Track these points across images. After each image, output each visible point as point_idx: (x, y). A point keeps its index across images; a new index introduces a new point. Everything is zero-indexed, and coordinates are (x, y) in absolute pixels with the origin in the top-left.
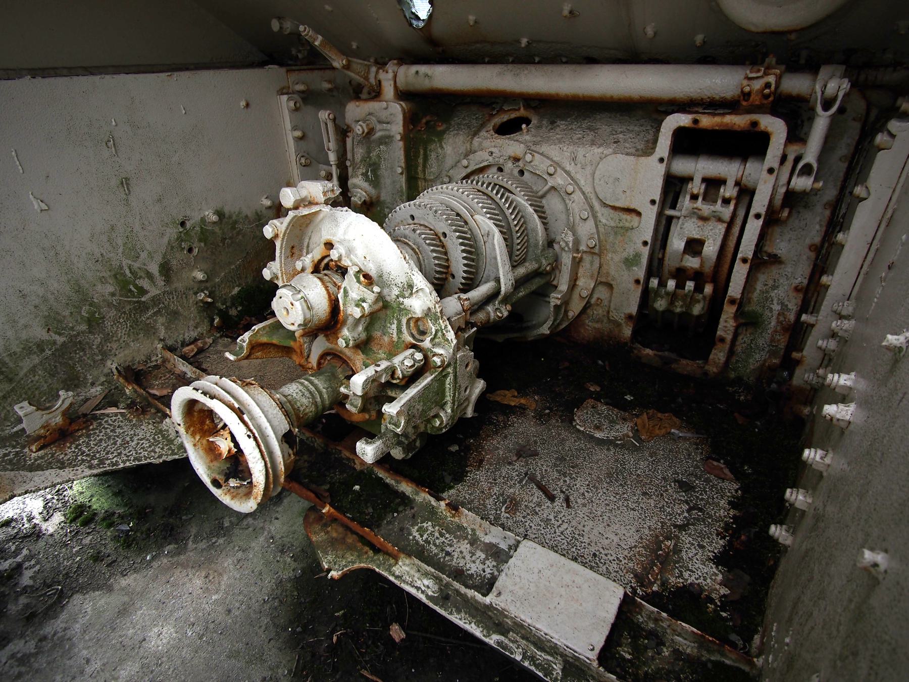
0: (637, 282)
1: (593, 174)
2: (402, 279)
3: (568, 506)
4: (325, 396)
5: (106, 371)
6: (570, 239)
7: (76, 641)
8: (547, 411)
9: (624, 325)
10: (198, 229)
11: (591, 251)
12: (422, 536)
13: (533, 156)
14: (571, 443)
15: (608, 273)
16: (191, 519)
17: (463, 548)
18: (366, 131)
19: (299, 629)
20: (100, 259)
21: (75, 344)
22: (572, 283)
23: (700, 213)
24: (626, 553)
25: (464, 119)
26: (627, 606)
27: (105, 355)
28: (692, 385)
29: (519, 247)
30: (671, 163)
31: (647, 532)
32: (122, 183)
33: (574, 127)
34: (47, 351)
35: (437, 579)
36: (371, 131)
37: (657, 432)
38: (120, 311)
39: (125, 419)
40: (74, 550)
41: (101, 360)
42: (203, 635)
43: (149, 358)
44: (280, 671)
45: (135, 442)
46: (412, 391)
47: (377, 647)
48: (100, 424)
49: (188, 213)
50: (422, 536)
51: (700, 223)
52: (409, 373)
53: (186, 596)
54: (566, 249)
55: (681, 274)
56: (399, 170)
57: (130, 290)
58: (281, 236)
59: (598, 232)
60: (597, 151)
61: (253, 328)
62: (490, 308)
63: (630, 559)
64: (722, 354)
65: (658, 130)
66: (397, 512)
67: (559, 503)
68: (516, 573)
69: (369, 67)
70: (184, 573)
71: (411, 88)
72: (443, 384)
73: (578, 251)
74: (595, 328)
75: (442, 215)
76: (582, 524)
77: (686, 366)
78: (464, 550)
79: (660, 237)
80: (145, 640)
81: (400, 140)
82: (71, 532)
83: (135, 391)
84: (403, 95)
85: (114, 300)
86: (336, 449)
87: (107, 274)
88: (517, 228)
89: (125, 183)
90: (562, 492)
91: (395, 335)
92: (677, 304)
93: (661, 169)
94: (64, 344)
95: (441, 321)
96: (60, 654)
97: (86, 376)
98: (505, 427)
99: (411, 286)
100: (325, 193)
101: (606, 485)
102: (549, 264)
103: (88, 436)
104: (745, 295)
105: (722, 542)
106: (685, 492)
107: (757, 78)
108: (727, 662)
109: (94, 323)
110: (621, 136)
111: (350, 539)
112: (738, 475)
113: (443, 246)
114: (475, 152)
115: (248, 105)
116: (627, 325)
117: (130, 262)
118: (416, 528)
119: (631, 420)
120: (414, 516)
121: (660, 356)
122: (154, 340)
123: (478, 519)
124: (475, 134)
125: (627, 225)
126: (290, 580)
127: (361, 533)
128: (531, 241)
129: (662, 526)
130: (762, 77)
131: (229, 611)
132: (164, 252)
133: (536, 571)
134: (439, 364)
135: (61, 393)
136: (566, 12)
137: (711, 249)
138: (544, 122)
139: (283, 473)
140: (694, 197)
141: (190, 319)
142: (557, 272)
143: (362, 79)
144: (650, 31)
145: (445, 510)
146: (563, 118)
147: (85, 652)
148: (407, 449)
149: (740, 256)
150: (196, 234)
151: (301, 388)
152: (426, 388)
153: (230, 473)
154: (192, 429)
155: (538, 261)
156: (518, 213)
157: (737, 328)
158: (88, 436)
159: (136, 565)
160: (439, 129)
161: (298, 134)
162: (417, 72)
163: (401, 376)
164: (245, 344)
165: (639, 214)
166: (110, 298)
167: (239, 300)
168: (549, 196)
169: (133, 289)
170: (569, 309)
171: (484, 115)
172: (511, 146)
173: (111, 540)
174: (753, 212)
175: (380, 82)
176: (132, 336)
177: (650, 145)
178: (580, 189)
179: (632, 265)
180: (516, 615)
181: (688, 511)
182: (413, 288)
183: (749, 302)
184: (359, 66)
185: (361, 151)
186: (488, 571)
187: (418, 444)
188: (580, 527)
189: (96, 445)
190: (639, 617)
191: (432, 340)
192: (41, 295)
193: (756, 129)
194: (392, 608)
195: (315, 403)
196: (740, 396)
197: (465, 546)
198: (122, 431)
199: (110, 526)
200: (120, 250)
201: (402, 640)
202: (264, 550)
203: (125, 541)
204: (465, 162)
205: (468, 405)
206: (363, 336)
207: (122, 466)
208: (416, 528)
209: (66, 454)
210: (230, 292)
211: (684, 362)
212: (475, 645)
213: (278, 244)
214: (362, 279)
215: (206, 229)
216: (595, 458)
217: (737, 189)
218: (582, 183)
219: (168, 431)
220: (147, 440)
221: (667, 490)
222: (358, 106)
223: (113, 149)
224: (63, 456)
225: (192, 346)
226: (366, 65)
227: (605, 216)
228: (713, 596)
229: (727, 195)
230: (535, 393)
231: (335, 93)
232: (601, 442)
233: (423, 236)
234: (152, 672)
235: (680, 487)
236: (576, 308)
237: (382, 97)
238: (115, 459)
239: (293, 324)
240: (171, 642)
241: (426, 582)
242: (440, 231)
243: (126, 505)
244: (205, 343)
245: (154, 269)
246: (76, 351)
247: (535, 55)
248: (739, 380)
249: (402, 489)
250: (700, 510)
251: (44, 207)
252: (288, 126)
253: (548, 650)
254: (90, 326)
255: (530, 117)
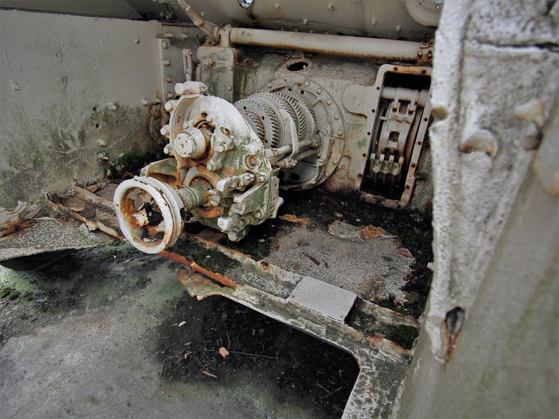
0: (364, 155)
1: (342, 95)
2: (244, 134)
3: (327, 267)
4: (198, 198)
5: (41, 195)
6: (329, 129)
7: (16, 362)
8: (314, 225)
9: (356, 180)
10: (103, 113)
11: (340, 137)
12: (248, 279)
13: (309, 83)
14: (327, 240)
15: (348, 150)
16: (86, 296)
17: (271, 284)
18: (211, 63)
19: (163, 352)
20: (45, 125)
21: (24, 176)
22: (329, 155)
23: (397, 118)
24: (357, 286)
25: (269, 61)
26: (358, 302)
27: (41, 185)
28: (392, 214)
29: (301, 131)
30: (383, 91)
31: (368, 278)
32: (63, 79)
33: (332, 69)
34: (8, 178)
35: (258, 295)
36: (213, 64)
37: (374, 236)
38: (53, 158)
39: (55, 224)
40: (7, 314)
41: (38, 188)
42: (101, 357)
43: (67, 191)
44: (152, 374)
45: (63, 236)
46: (249, 193)
47: (212, 359)
48: (39, 226)
49: (98, 103)
50: (248, 279)
51: (397, 123)
52: (247, 184)
53: (88, 337)
54: (327, 134)
55: (387, 151)
56: (230, 88)
57: (60, 146)
58: (175, 109)
59: (344, 127)
60: (345, 82)
61: (150, 164)
62: (286, 160)
63: (360, 289)
64: (408, 195)
65: (376, 73)
66: (233, 268)
67: (322, 265)
68: (301, 289)
69: (214, 27)
70: (85, 325)
71: (239, 41)
72: (263, 193)
73: (332, 137)
74: (340, 182)
75: (262, 106)
76: (334, 274)
77: (389, 203)
78: (272, 284)
79: (376, 133)
80: (63, 360)
81: (231, 70)
82: (2, 303)
83: (60, 209)
84: (235, 45)
85: (51, 151)
86: (194, 238)
87: (48, 134)
88: (301, 120)
89: (65, 80)
90: (323, 261)
91: (238, 166)
92: (385, 169)
93: (378, 93)
94: (18, 175)
95: (264, 158)
96: (5, 369)
97: (28, 197)
98: (290, 232)
99: (249, 139)
100: (200, 88)
101: (346, 258)
102: (317, 142)
103: (33, 231)
104: (420, 163)
105: (406, 282)
106: (388, 261)
107: (425, 48)
108: (406, 324)
109: (37, 164)
110: (357, 75)
111: (206, 281)
112: (414, 254)
113: (262, 124)
114: (276, 79)
115: (139, 42)
116: (358, 180)
117: (62, 129)
118: (244, 275)
119: (360, 230)
120: (242, 270)
121: (376, 198)
122: (70, 180)
123: (279, 269)
124: (276, 69)
125: (360, 123)
126: (155, 328)
127: (213, 277)
128: (307, 129)
129: (376, 276)
130: (427, 48)
131: (117, 344)
132: (82, 125)
133: (312, 288)
134: (263, 180)
135: (19, 202)
136: (330, 7)
137: (402, 138)
138: (315, 66)
139: (180, 229)
140: (395, 110)
141: (93, 169)
142: (321, 148)
143: (210, 34)
144: (373, 22)
145: (260, 266)
146: (326, 64)
147: (23, 368)
148: (239, 235)
149: (417, 141)
150: (101, 116)
151: (185, 191)
152: (256, 192)
153: (143, 236)
154: (124, 209)
155: (311, 140)
156: (301, 112)
157: (416, 180)
158: (33, 231)
159: (51, 321)
160: (255, 65)
161: (167, 62)
162: (243, 32)
163: (243, 185)
164: (146, 172)
165: (366, 117)
166: (48, 149)
167: (123, 161)
168: (317, 106)
169: (62, 146)
170: (326, 171)
171: (280, 59)
172: (297, 77)
173: (32, 308)
174: (423, 117)
175: (220, 36)
176: (58, 176)
177: (372, 81)
178: (335, 102)
179: (362, 145)
180: (303, 305)
181: (389, 270)
182: (250, 139)
183: (422, 168)
184: (209, 25)
185: (206, 75)
186: (285, 293)
187: (244, 233)
188: (333, 276)
189: (38, 237)
190: (364, 309)
191: (259, 168)
192: (9, 142)
193: (425, 74)
194: (219, 341)
195: (193, 200)
196: (417, 219)
197: (272, 283)
198: (54, 230)
199: (31, 299)
200: (57, 121)
201: (227, 356)
202: (137, 313)
203: (42, 308)
204: (270, 85)
205: (274, 210)
206: (220, 165)
207: (56, 249)
208: (244, 275)
209: (19, 241)
210: (118, 155)
211: (388, 200)
212: (270, 357)
213: (172, 114)
214: (225, 131)
215: (108, 114)
216: (340, 247)
217: (416, 106)
218: (336, 99)
219: (83, 231)
220: (71, 236)
221: (378, 261)
222: (205, 49)
223: (60, 58)
224: (18, 241)
225: (94, 186)
226: (212, 25)
227: (348, 118)
228: (401, 303)
229: (411, 109)
230: (306, 217)
231: (189, 41)
232: (343, 240)
233: (252, 117)
234: (70, 376)
235: (385, 260)
236: (330, 170)
237: (221, 45)
238: (52, 245)
239: (185, 153)
240: (81, 361)
241: (252, 298)
242: (261, 116)
243: (40, 289)
244: (101, 185)
245: (76, 135)
246: (24, 180)
247: (311, 29)
248: (416, 210)
249: (235, 257)
250: (395, 269)
251: (17, 88)
252: (161, 57)
253: (319, 323)
254: (35, 165)
255: (307, 63)
